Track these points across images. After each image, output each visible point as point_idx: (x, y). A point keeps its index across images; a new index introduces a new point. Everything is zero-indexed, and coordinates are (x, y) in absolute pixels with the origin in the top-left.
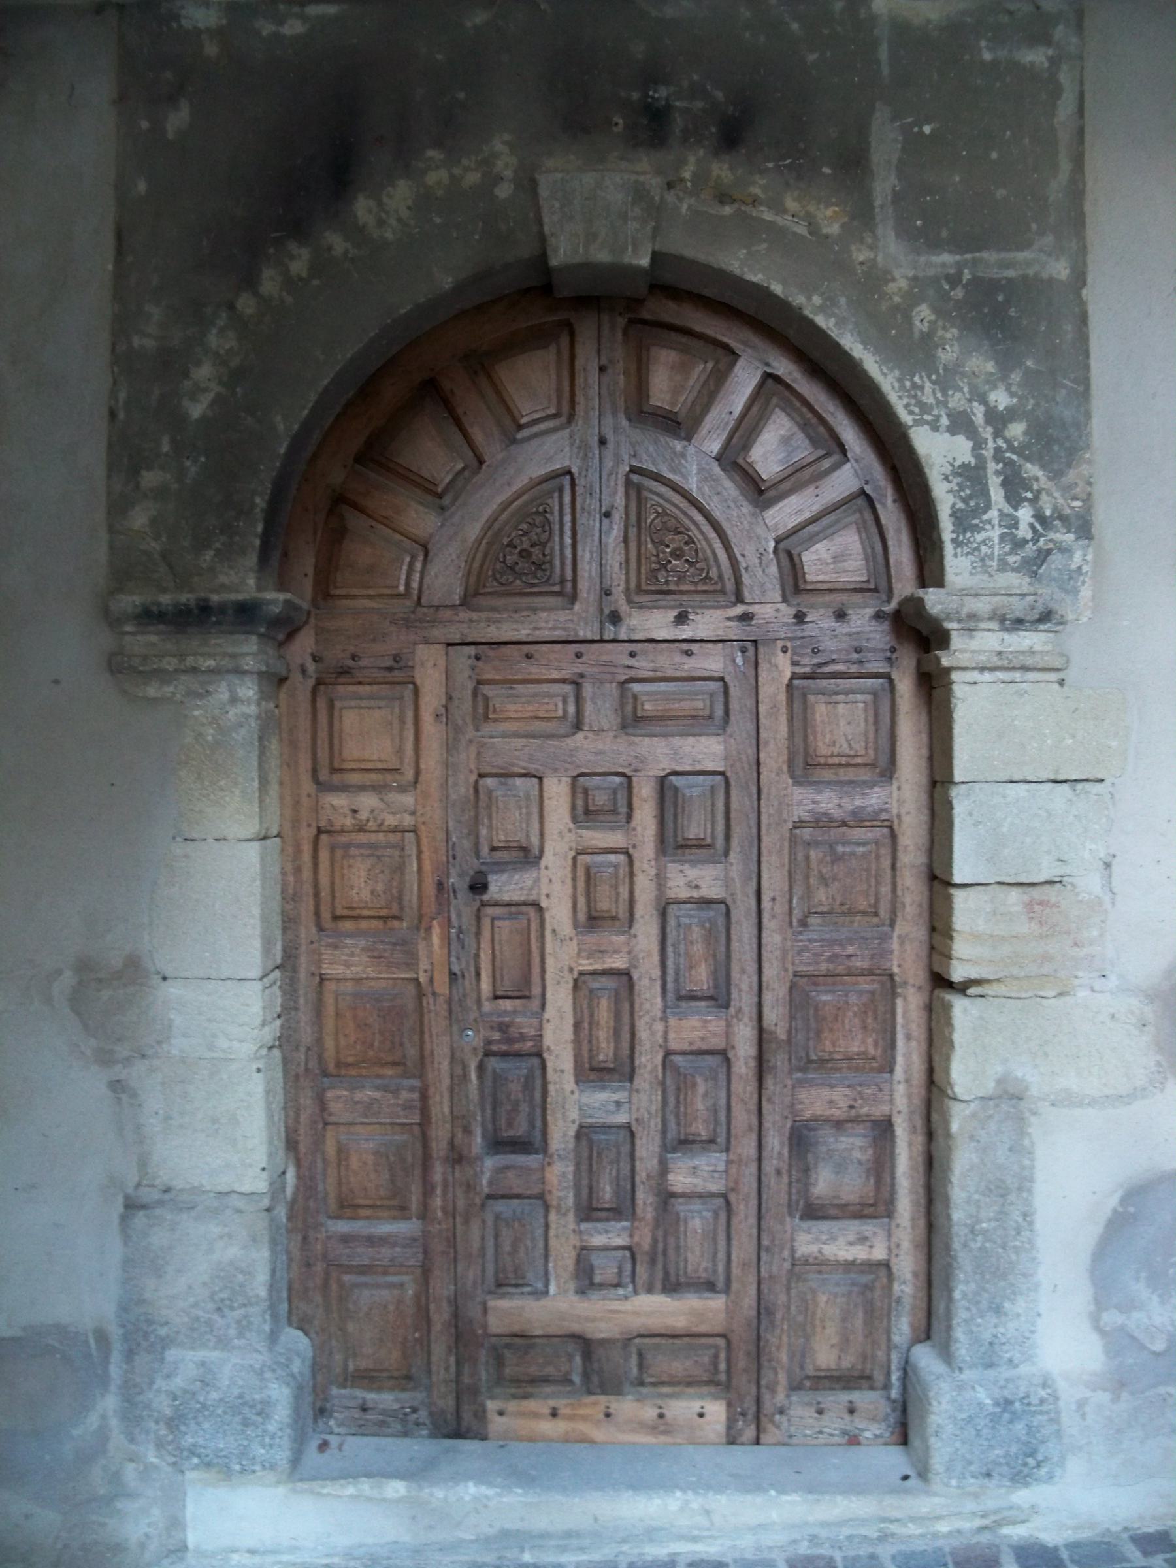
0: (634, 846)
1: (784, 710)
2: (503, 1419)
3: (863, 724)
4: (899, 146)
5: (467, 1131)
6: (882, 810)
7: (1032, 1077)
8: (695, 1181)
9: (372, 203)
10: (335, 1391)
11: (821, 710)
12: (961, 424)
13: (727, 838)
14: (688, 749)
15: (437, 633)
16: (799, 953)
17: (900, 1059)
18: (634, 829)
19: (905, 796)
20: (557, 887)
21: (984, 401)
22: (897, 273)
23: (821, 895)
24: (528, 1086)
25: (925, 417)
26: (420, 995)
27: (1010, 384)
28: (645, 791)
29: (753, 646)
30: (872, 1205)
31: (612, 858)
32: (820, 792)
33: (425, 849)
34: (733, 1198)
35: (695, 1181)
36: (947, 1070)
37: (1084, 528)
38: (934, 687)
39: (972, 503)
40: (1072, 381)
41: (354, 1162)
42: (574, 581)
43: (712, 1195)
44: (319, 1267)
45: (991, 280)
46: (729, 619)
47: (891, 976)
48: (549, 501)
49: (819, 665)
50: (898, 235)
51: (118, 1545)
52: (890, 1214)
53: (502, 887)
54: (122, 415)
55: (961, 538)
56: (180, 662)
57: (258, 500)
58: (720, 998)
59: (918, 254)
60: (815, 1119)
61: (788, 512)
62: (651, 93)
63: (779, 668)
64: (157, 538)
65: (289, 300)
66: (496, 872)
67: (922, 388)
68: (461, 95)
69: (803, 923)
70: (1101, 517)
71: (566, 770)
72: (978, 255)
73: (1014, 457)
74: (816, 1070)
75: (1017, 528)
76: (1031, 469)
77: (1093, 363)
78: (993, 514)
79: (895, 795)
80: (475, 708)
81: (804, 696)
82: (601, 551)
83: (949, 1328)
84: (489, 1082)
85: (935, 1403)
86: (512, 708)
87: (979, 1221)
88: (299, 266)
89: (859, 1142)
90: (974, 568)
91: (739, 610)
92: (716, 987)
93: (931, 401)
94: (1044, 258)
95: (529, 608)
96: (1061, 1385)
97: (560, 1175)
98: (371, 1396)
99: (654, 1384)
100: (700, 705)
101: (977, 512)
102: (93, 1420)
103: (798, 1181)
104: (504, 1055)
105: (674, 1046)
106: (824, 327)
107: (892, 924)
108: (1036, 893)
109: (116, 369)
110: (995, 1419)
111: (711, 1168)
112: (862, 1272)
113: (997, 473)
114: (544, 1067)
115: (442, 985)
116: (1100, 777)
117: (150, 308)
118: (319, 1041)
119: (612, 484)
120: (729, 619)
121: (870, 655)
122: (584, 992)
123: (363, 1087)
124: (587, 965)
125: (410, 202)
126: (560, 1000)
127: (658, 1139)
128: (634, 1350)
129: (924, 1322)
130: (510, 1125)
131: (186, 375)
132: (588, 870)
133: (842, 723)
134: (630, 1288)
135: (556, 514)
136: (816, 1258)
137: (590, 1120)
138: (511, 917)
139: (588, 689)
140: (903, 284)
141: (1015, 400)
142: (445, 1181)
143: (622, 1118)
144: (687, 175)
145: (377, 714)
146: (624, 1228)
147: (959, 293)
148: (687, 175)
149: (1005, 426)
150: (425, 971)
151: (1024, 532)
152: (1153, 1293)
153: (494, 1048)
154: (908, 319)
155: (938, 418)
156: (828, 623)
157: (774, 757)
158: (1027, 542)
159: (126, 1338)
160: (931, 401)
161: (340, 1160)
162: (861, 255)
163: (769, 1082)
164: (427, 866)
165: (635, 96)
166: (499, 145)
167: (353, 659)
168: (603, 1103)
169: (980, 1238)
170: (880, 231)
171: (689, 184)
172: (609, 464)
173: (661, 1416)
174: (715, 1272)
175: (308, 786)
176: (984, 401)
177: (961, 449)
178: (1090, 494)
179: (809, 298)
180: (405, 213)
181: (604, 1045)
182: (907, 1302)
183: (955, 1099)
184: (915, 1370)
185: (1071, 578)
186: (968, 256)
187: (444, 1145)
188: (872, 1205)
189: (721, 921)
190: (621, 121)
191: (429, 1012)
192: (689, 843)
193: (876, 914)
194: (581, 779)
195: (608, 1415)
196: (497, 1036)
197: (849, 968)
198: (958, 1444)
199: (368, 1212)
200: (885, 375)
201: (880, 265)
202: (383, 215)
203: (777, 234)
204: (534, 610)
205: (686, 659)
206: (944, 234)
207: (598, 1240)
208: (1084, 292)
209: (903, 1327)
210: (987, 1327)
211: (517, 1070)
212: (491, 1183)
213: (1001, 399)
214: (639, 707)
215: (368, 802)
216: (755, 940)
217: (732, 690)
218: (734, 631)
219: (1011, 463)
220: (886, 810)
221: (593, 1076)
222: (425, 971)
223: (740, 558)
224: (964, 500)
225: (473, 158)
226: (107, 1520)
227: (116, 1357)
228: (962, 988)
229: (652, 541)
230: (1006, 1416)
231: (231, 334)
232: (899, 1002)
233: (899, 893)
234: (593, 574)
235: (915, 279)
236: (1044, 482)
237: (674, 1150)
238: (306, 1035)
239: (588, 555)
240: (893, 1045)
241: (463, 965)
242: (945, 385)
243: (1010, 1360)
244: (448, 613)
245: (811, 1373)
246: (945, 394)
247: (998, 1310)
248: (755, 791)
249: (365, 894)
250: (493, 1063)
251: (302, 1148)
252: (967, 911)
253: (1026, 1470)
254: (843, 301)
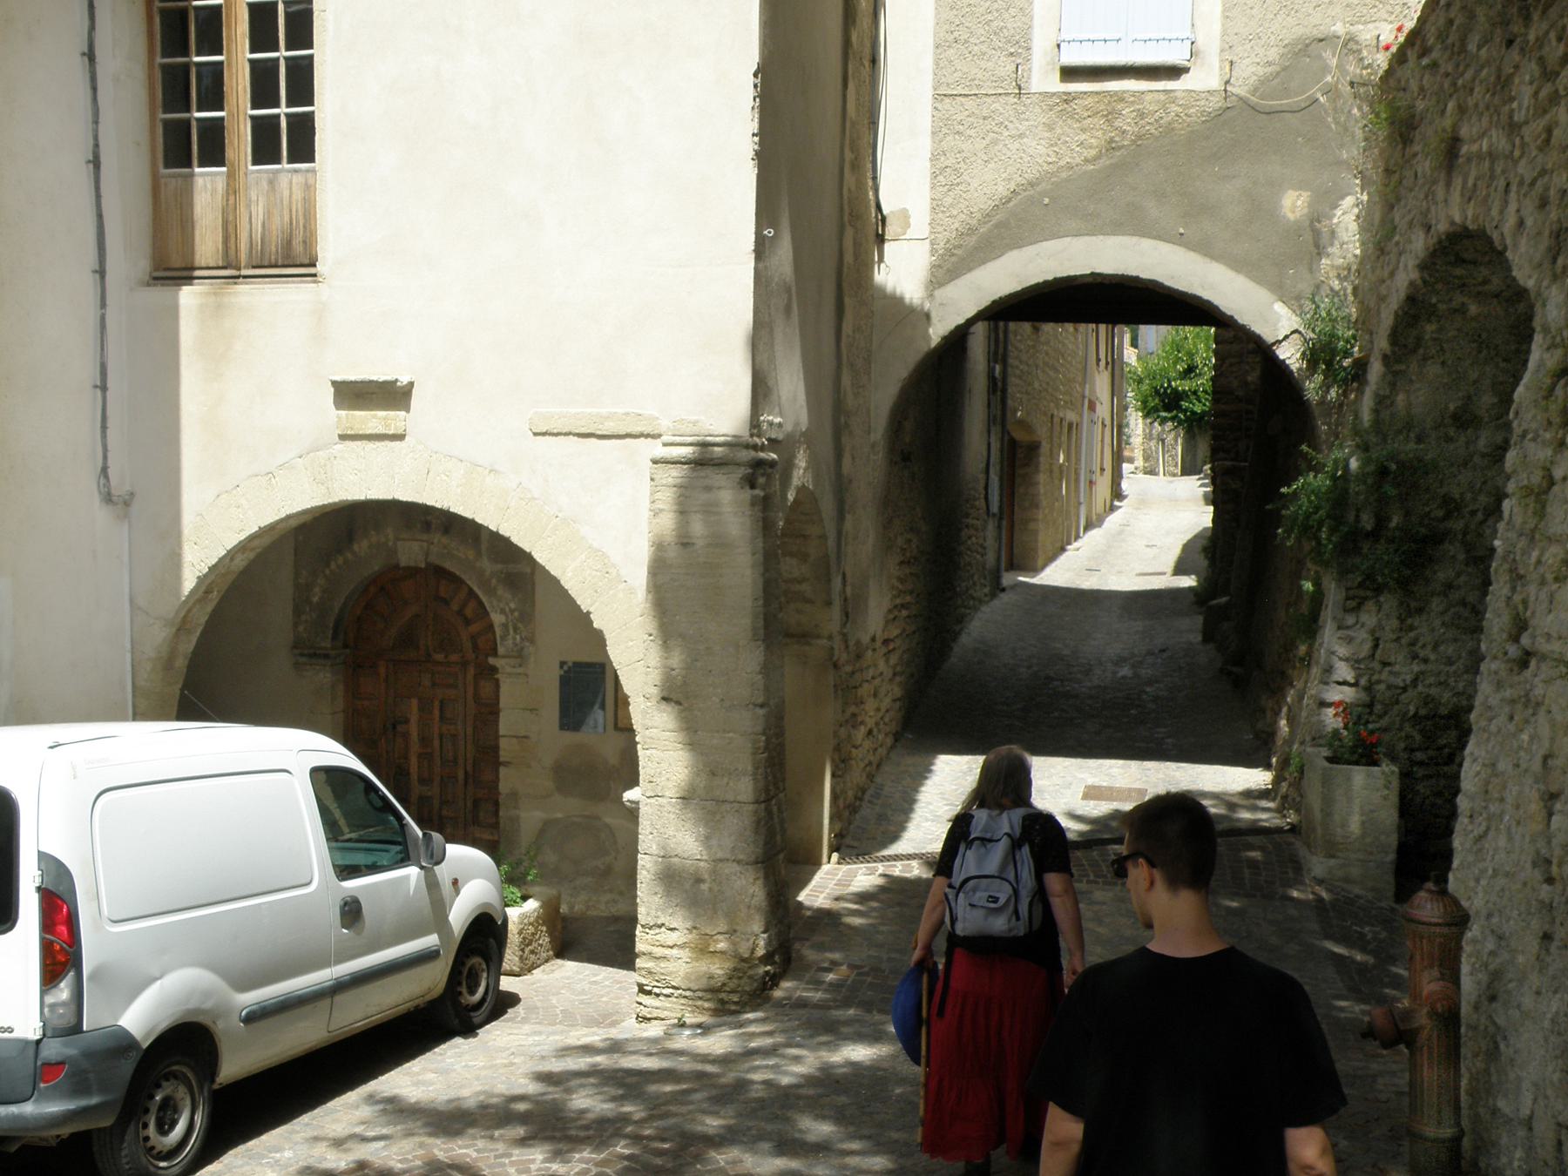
12: (503, 611)
37: (532, 641)
53: (399, 728)
126: (414, 761)
213: (513, 606)
215: (366, 703)
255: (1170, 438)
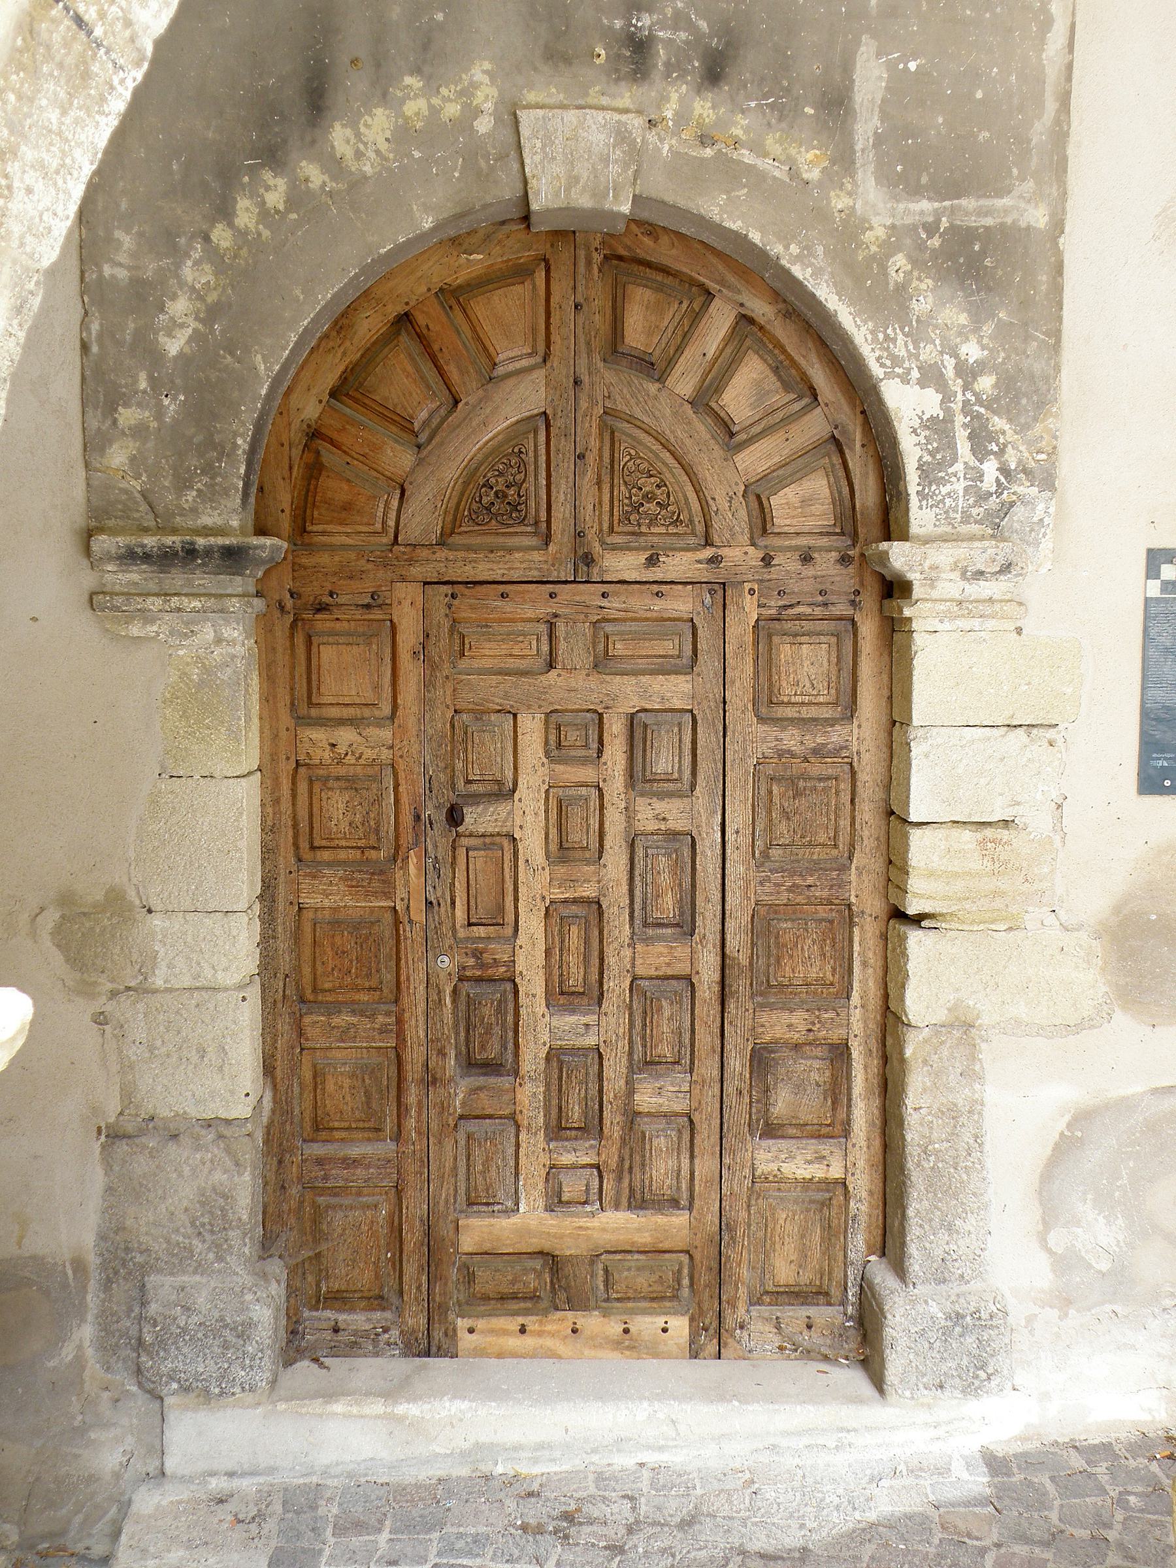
0: (604, 780)
1: (750, 650)
2: (473, 1337)
3: (825, 664)
4: (883, 84)
5: (442, 1053)
6: (842, 748)
7: (988, 1011)
8: (661, 1101)
9: (348, 132)
10: (306, 1314)
11: (785, 651)
12: (931, 377)
13: (694, 773)
14: (657, 687)
15: (416, 571)
16: (761, 883)
17: (856, 985)
18: (605, 764)
19: (863, 735)
20: (529, 818)
21: (955, 355)
22: (875, 221)
23: (782, 827)
24: (500, 1011)
25: (897, 370)
26: (397, 922)
27: (982, 337)
28: (616, 727)
29: (721, 590)
30: (829, 1125)
31: (583, 791)
32: (784, 729)
33: (402, 781)
34: (696, 1118)
35: (661, 1101)
36: (902, 999)
37: (1048, 482)
38: (895, 635)
39: (939, 456)
40: (1044, 334)
41: (330, 1086)
42: (549, 522)
43: (676, 1115)
44: (294, 1191)
45: (968, 228)
46: (699, 562)
47: (849, 906)
48: (525, 442)
49: (785, 607)
50: (878, 182)
51: (91, 1476)
52: (846, 1133)
53: (478, 819)
54: (95, 349)
55: (927, 491)
56: (165, 602)
57: (240, 441)
58: (686, 926)
59: (898, 201)
60: (776, 1042)
61: (755, 460)
62: (634, 21)
63: (747, 610)
64: (137, 477)
65: (266, 233)
66: (471, 805)
67: (894, 340)
68: (440, 17)
69: (765, 855)
70: (1064, 469)
71: (540, 707)
72: (956, 202)
73: (982, 410)
74: (775, 994)
75: (982, 482)
76: (998, 423)
77: (1065, 313)
78: (959, 467)
79: (855, 731)
80: (451, 645)
81: (770, 636)
82: (576, 498)
83: (903, 1244)
84: (462, 1007)
85: (889, 1317)
86: (489, 648)
87: (931, 1142)
88: (275, 198)
89: (817, 1064)
90: (938, 520)
91: (708, 552)
92: (682, 914)
93: (903, 353)
94: (1022, 205)
95: (504, 548)
96: (1012, 1303)
97: (530, 1096)
98: (342, 1317)
99: (618, 1300)
100: (668, 647)
101: (941, 465)
102: (68, 1352)
103: (758, 1101)
104: (479, 980)
105: (640, 971)
106: (801, 278)
107: (850, 858)
108: (989, 832)
109: (86, 299)
110: (946, 1332)
111: (676, 1089)
112: (818, 1190)
113: (965, 426)
114: (516, 992)
115: (418, 913)
116: (1054, 722)
117: (118, 234)
118: (298, 969)
119: (587, 425)
120: (699, 562)
121: (833, 598)
122: (555, 919)
123: (339, 1012)
124: (559, 894)
125: (388, 134)
126: (532, 926)
127: (624, 1060)
128: (601, 1266)
129: (879, 1239)
130: (483, 1047)
131: (162, 309)
132: (560, 802)
133: (807, 666)
134: (597, 1205)
135: (531, 454)
136: (775, 1176)
137: (559, 1043)
138: (485, 847)
139: (561, 629)
140: (881, 232)
141: (986, 352)
142: (420, 1102)
143: (591, 1040)
144: (669, 114)
145: (355, 650)
146: (592, 1147)
147: (935, 242)
148: (669, 114)
149: (975, 378)
150: (402, 900)
151: (989, 484)
152: (1099, 1214)
153: (468, 974)
154: (884, 269)
155: (908, 371)
156: (794, 565)
157: (740, 695)
158: (991, 495)
159: (104, 1266)
160: (903, 353)
161: (316, 1084)
162: (839, 202)
163: (731, 1006)
164: (404, 799)
165: (618, 24)
166: (479, 72)
167: (331, 596)
168: (571, 1027)
169: (932, 1158)
170: (860, 175)
171: (670, 123)
172: (584, 405)
173: (626, 1331)
174: (679, 1188)
175: (286, 720)
176: (955, 355)
177: (930, 402)
178: (1055, 448)
179: (787, 247)
180: (383, 146)
181: (573, 970)
182: (863, 1219)
183: (909, 1025)
184: (871, 1287)
185: (1032, 530)
186: (947, 203)
187: (419, 1067)
188: (829, 1125)
189: (687, 852)
190: (603, 52)
191: (406, 939)
192: (658, 777)
193: (835, 846)
194: (554, 715)
195: (574, 1331)
196: (471, 962)
197: (808, 897)
198: (911, 1357)
199: (343, 1134)
200: (858, 327)
201: (859, 213)
202: (361, 147)
203: (758, 178)
204: (510, 550)
205: (657, 601)
206: (924, 180)
207: (567, 1159)
208: (1061, 240)
209: (859, 1243)
210: (939, 1243)
211: (489, 995)
212: (463, 1104)
213: (972, 351)
214: (611, 646)
215: (346, 736)
216: (719, 871)
217: (700, 632)
218: (702, 573)
219: (979, 416)
220: (846, 747)
221: (563, 1000)
222: (402, 900)
223: (711, 502)
224: (930, 453)
225: (452, 87)
226: (80, 1452)
227: (92, 1285)
228: (917, 920)
229: (625, 483)
230: (958, 1329)
231: (207, 267)
232: (856, 930)
233: (857, 826)
234: (567, 515)
235: (893, 227)
236: (1010, 436)
237: (640, 1071)
238: (285, 962)
239: (562, 497)
240: (850, 971)
241: (439, 894)
242: (917, 337)
243: (962, 1276)
244: (424, 553)
245: (771, 1288)
246: (916, 347)
247: (950, 1228)
248: (721, 728)
249: (344, 826)
250: (466, 987)
251: (279, 1073)
252: (922, 849)
253: (977, 1383)
254: (820, 250)
255: (817, 509)
